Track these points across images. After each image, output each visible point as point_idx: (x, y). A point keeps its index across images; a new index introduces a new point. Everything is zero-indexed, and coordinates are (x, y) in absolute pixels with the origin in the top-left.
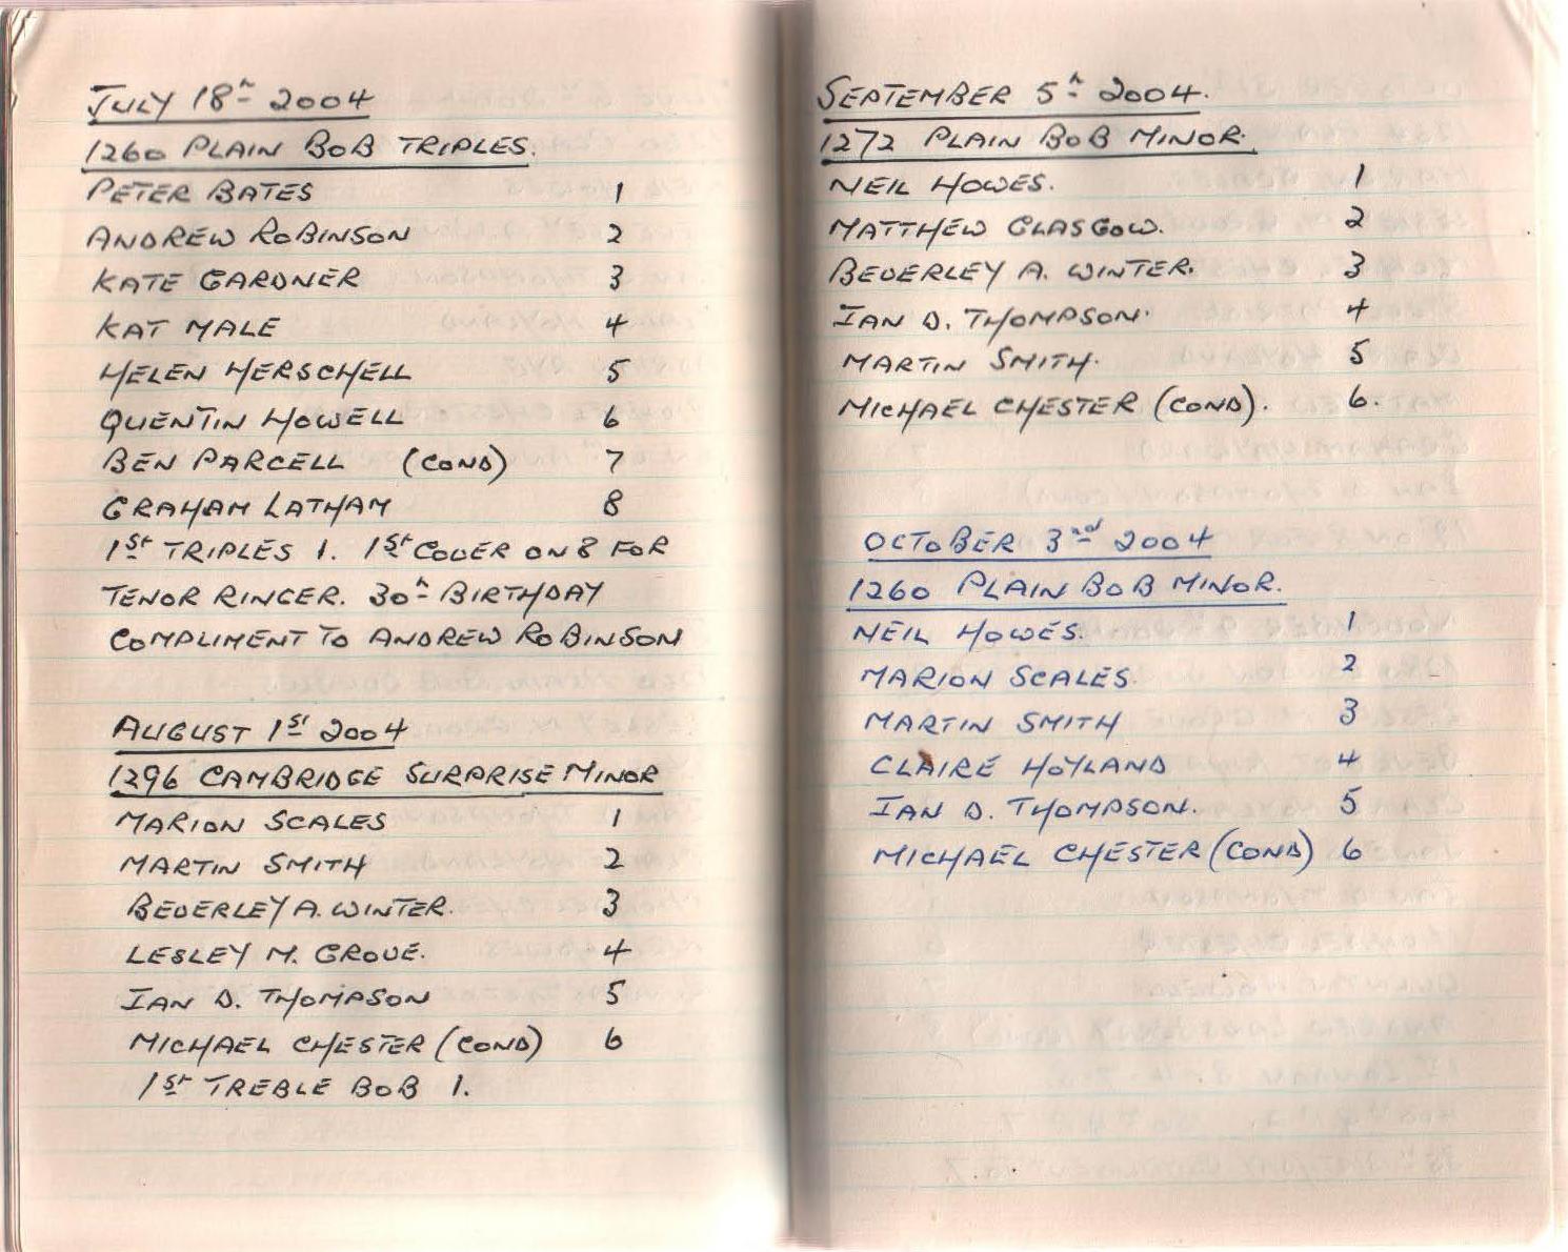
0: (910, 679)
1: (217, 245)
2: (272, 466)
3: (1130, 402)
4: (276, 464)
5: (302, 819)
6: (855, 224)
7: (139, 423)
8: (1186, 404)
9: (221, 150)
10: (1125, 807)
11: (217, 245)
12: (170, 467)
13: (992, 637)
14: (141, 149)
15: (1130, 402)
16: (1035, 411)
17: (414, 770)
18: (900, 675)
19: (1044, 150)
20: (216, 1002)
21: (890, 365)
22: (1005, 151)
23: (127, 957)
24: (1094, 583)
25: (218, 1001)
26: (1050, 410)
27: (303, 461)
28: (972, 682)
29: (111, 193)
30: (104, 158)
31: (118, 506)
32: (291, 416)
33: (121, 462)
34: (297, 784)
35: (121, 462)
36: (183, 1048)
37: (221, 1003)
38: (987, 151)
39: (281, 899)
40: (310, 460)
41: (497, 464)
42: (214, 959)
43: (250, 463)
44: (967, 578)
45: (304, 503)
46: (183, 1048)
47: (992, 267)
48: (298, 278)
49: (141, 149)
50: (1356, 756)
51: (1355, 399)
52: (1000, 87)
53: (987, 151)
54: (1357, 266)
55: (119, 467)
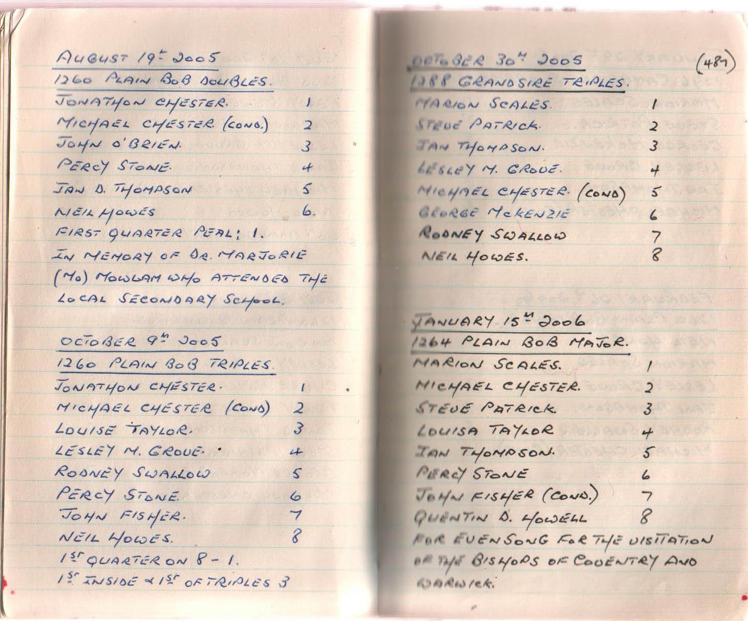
0: (246, 256)
1: (129, 215)
2: (158, 103)
3: (531, 494)
4: (523, 127)
5: (525, 125)
6: (98, 254)
7: (127, 234)
8: (560, 495)
9: (122, 80)
10: (164, 189)
11: (129, 215)
12: (127, 449)
13: (196, 280)
14: (84, 362)
15: (531, 494)
16: (519, 194)
17: (229, 297)
18: (467, 386)
19: (202, 87)
20: (500, 519)
21: (470, 387)
22: (149, 370)
23: (56, 430)
24: (167, 77)
25: (501, 519)
26: (478, 193)
27: (521, 495)
28: (540, 454)
29: (71, 166)
30: (65, 366)
31: (157, 450)
32: (177, 101)
33: (110, 342)
34: (163, 454)
35: (172, 364)
36: (239, 301)
37: (502, 519)
38: (140, 370)
39: (149, 254)
40: (571, 517)
41: (620, 193)
42: (521, 475)
43: (545, 430)
44: (594, 501)
45: (153, 231)
46: (239, 301)
47: (104, 163)
48: (532, 148)
49: (84, 362)
50: (449, 341)
51: (578, 322)
52: (86, 163)
53: (140, 370)
54: (300, 428)
55: (109, 344)
